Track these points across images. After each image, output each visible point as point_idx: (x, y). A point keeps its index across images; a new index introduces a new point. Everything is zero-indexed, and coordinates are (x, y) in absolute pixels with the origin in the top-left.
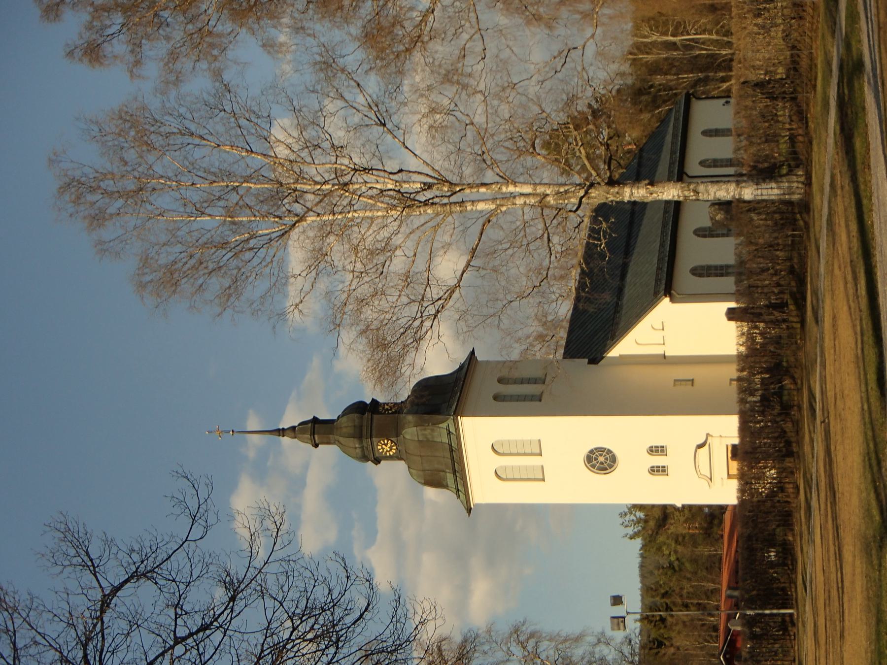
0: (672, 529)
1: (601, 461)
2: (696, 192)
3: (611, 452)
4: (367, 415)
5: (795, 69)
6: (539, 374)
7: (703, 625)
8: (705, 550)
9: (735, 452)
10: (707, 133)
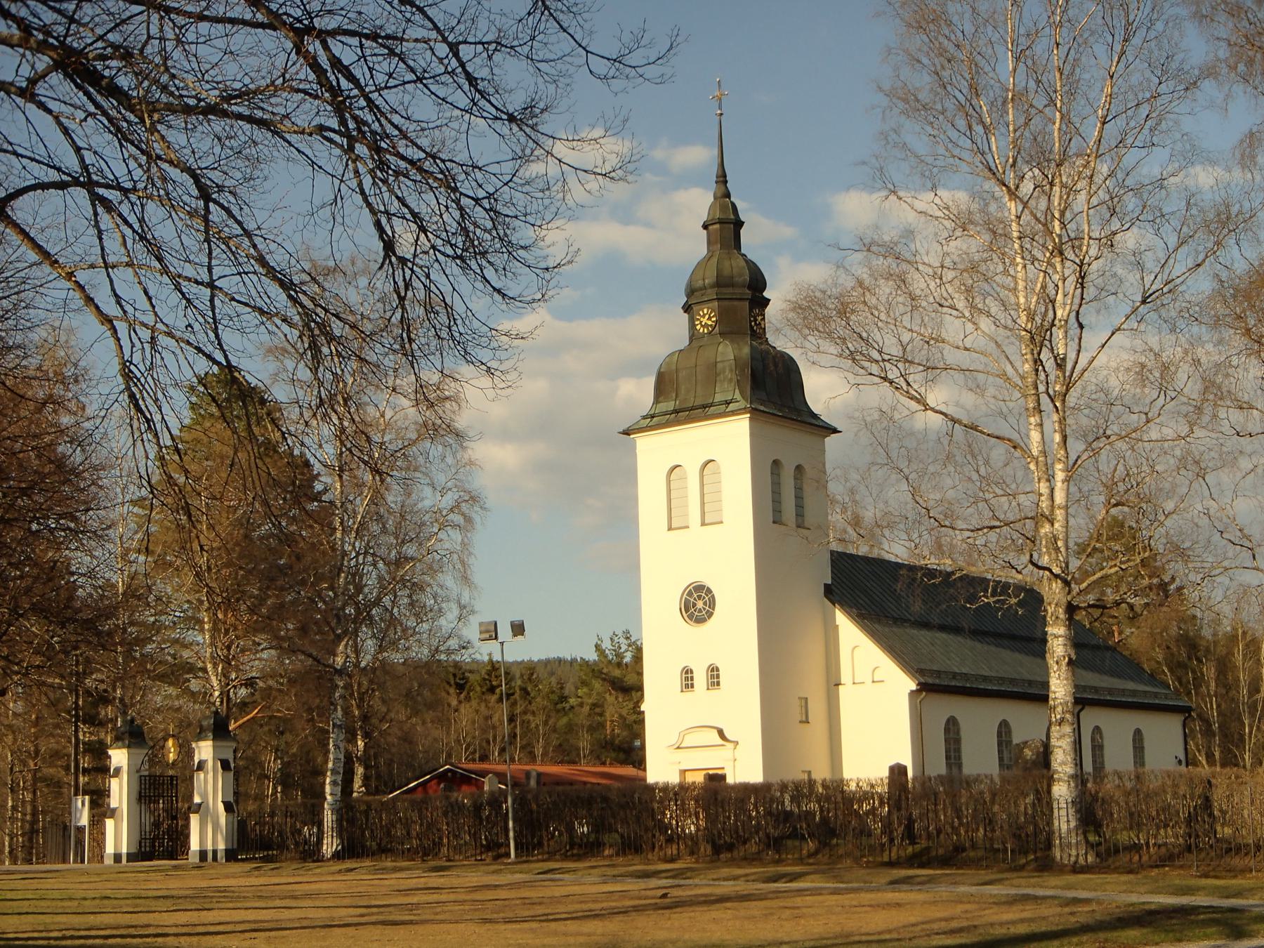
0: (610, 699)
1: (698, 604)
2: (1061, 722)
3: (710, 617)
4: (748, 293)
5: (1229, 850)
6: (810, 519)
7: (488, 742)
8: (584, 742)
9: (716, 779)
10: (1138, 736)
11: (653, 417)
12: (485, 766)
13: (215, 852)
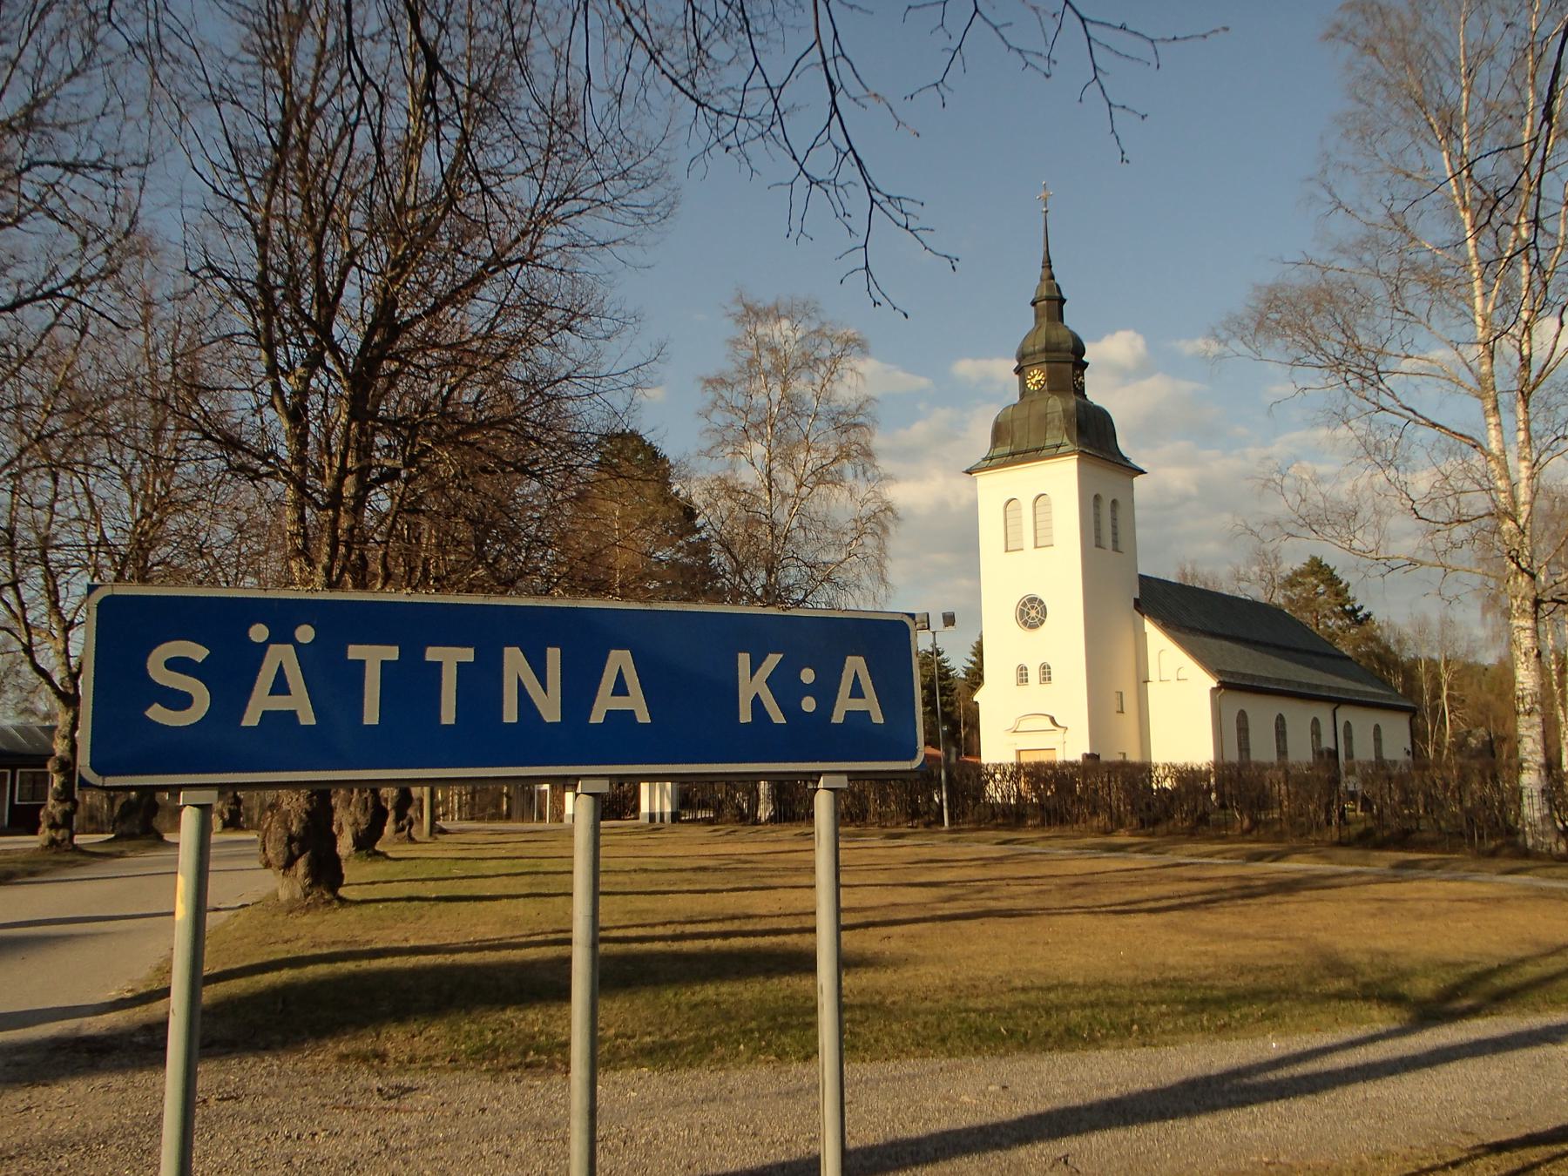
1: (1032, 613)
2: (1529, 713)
4: (1072, 357)
6: (1122, 546)
10: (1377, 729)
13: (662, 815)
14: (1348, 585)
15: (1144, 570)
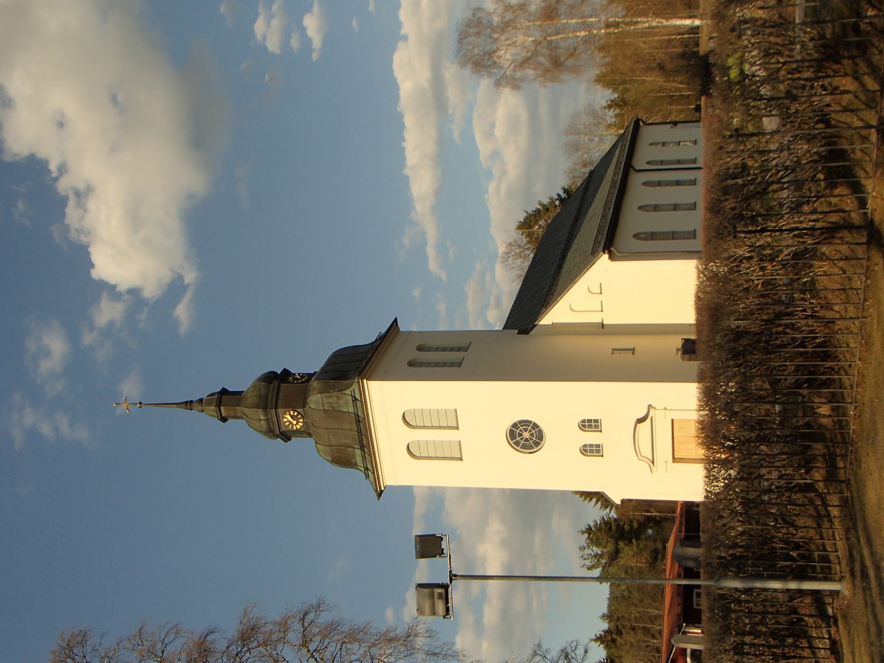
1: (526, 436)
3: (537, 426)
7: (648, 646)
11: (367, 469)
12: (664, 648)
14: (540, 204)
15: (499, 326)
